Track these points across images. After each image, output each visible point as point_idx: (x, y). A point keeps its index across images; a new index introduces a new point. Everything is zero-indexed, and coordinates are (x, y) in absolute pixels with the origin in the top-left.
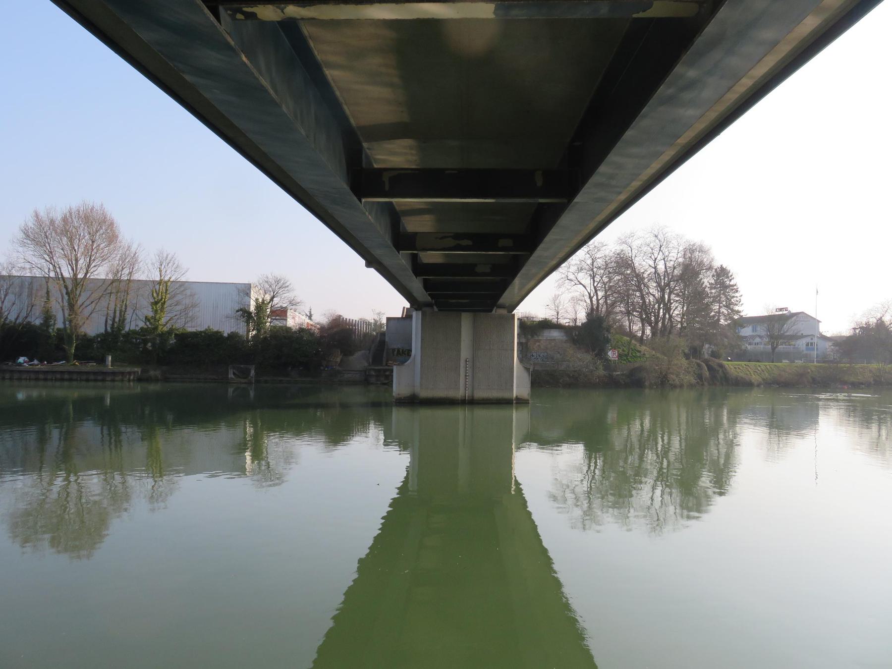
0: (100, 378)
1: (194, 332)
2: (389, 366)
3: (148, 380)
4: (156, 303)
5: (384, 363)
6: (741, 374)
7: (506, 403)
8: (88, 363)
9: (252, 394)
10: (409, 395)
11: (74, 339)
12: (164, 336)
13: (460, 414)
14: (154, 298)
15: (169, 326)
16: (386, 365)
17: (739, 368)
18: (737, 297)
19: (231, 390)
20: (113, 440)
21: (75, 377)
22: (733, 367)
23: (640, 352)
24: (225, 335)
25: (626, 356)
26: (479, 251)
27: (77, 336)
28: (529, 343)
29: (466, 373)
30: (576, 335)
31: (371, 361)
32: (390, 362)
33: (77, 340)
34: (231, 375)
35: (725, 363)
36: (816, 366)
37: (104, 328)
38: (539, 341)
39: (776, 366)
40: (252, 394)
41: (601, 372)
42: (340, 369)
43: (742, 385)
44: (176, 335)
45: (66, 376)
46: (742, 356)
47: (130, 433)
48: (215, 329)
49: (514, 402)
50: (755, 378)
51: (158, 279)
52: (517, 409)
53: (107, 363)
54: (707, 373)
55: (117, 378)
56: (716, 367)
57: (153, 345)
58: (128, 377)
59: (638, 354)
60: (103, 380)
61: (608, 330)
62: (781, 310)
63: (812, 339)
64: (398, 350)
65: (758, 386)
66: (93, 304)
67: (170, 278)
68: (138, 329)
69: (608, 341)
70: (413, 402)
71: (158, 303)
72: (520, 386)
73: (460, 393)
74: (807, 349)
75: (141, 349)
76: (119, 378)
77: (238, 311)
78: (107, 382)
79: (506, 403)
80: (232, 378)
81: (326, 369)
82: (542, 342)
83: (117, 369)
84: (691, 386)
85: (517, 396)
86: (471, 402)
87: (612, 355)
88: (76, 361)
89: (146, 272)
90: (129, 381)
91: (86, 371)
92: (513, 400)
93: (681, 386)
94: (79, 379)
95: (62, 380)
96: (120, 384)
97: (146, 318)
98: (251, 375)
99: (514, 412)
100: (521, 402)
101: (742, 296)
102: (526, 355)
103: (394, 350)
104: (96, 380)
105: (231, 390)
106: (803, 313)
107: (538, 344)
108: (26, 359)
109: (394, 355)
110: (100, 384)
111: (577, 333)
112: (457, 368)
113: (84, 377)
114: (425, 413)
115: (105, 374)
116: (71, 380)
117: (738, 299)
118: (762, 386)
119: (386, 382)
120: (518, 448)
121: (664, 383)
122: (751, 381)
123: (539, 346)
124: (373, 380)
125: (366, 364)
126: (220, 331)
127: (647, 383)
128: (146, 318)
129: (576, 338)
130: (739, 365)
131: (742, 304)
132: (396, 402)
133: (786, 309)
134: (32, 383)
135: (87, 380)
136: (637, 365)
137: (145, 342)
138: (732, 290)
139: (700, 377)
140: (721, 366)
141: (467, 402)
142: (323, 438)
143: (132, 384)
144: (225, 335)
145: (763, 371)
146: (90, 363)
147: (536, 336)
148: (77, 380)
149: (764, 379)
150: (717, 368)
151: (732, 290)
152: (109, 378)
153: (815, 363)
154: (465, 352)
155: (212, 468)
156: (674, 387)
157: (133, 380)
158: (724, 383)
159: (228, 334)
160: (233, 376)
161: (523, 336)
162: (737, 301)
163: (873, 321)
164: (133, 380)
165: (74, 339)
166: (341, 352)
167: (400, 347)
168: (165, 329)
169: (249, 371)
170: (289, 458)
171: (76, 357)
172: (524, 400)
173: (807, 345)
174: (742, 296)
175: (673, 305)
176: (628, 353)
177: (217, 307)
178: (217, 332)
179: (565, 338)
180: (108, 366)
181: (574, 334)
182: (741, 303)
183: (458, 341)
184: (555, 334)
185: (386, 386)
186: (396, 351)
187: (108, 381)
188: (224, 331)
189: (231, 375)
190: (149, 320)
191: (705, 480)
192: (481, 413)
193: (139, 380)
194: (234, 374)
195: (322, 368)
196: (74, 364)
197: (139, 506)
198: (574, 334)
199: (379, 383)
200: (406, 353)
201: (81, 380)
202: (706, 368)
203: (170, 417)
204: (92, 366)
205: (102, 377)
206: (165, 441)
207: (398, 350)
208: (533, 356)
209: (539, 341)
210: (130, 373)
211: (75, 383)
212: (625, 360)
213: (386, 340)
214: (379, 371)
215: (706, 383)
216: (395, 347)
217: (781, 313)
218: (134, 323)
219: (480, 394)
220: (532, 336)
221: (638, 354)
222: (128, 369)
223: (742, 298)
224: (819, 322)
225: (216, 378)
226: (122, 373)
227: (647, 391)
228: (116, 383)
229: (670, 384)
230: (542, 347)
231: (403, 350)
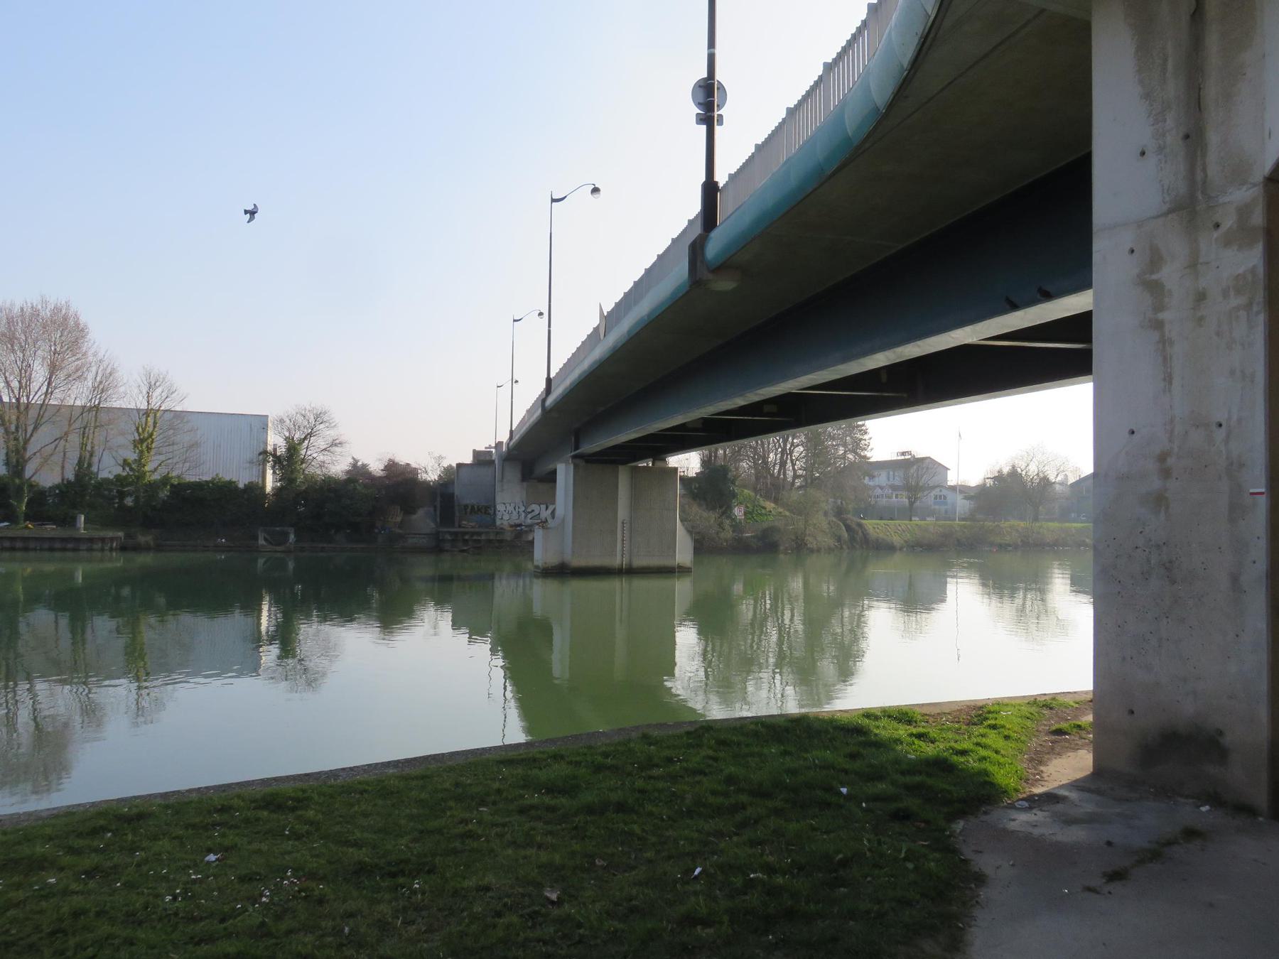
0: (70, 546)
1: (196, 482)
2: (464, 527)
3: (137, 548)
4: (142, 441)
5: (457, 524)
6: (881, 535)
8: (44, 525)
9: (291, 565)
11: (26, 492)
12: (154, 487)
13: (616, 586)
14: (139, 435)
15: (163, 471)
16: (460, 526)
17: (878, 528)
18: (865, 440)
19: (261, 562)
21: (32, 545)
22: (873, 526)
23: (765, 508)
24: (241, 486)
25: (751, 513)
26: (745, 416)
27: (31, 486)
29: (623, 537)
31: (438, 520)
32: (464, 522)
33: (29, 491)
34: (261, 542)
35: (864, 522)
36: (958, 525)
37: (32, 474)
39: (917, 525)
40: (291, 565)
41: (728, 534)
42: (400, 531)
43: (883, 548)
44: (172, 486)
46: (886, 514)
47: (102, 626)
48: (227, 479)
50: (897, 540)
51: (144, 406)
52: (678, 579)
53: (78, 525)
54: (845, 535)
55: (95, 546)
56: (854, 526)
57: (137, 500)
58: (109, 545)
59: (763, 511)
60: (75, 550)
61: (733, 482)
62: (903, 454)
63: (941, 491)
64: (473, 507)
65: (901, 549)
66: (58, 441)
67: (160, 407)
68: (111, 477)
69: (734, 495)
71: (143, 442)
72: (683, 553)
73: (617, 561)
74: (935, 504)
75: (116, 505)
76: (98, 546)
78: (81, 552)
80: (263, 545)
81: (383, 532)
84: (830, 550)
85: (678, 564)
86: (630, 572)
87: (738, 512)
88: (28, 522)
89: (129, 397)
91: (50, 536)
93: (819, 550)
94: (38, 548)
95: (13, 549)
96: (99, 554)
97: (125, 461)
98: (291, 541)
100: (682, 571)
101: (871, 438)
103: (466, 506)
104: (64, 550)
105: (261, 562)
106: (929, 458)
109: (466, 513)
110: (70, 554)
111: (697, 486)
112: (614, 532)
113: (46, 546)
114: (577, 585)
115: (78, 540)
116: (26, 549)
117: (866, 443)
118: (905, 549)
119: (465, 548)
121: (800, 547)
122: (893, 543)
124: (447, 546)
125: (433, 525)
126: (234, 480)
127: (782, 548)
128: (125, 461)
129: (696, 491)
130: (878, 524)
131: (872, 449)
133: (909, 453)
134: (47, 554)
135: (51, 549)
136: (765, 525)
137: (122, 495)
138: (860, 431)
139: (839, 539)
140: (860, 525)
141: (624, 571)
142: (976, 581)
143: (114, 554)
144: (241, 486)
145: (904, 531)
146: (47, 524)
148: (35, 550)
149: (906, 542)
150: (857, 528)
151: (860, 431)
152: (83, 547)
153: (957, 522)
154: (623, 512)
155: (222, 667)
156: (812, 551)
157: (116, 549)
158: (865, 547)
159: (245, 485)
160: (264, 543)
162: (865, 445)
163: (1006, 470)
164: (116, 549)
165: (26, 492)
166: (401, 510)
167: (475, 503)
168: (156, 477)
169: (286, 535)
170: (329, 651)
171: (28, 517)
172: (686, 568)
173: (936, 498)
174: (871, 438)
175: (797, 449)
176: (753, 510)
177: (220, 447)
178: (231, 482)
180: (79, 529)
181: (693, 487)
182: (870, 447)
185: (465, 554)
186: (470, 508)
187: (83, 550)
188: (239, 481)
189: (261, 542)
190: (129, 465)
191: (827, 667)
192: (640, 584)
193: (123, 549)
194: (266, 539)
195: (376, 531)
196: (27, 527)
197: (117, 725)
198: (693, 487)
199: (455, 549)
200: (483, 511)
201: (41, 550)
202: (844, 528)
203: (161, 601)
204: (50, 530)
205: (73, 545)
206: (150, 630)
210: (112, 539)
211: (32, 554)
212: (750, 519)
213: (456, 493)
214: (456, 534)
215: (844, 547)
216: (468, 502)
217: (903, 457)
218: (107, 468)
219: (639, 562)
221: (763, 511)
223: (871, 441)
224: (947, 469)
225: (232, 545)
226: (103, 540)
227: (782, 556)
228: (94, 554)
229: (808, 549)
231: (478, 507)
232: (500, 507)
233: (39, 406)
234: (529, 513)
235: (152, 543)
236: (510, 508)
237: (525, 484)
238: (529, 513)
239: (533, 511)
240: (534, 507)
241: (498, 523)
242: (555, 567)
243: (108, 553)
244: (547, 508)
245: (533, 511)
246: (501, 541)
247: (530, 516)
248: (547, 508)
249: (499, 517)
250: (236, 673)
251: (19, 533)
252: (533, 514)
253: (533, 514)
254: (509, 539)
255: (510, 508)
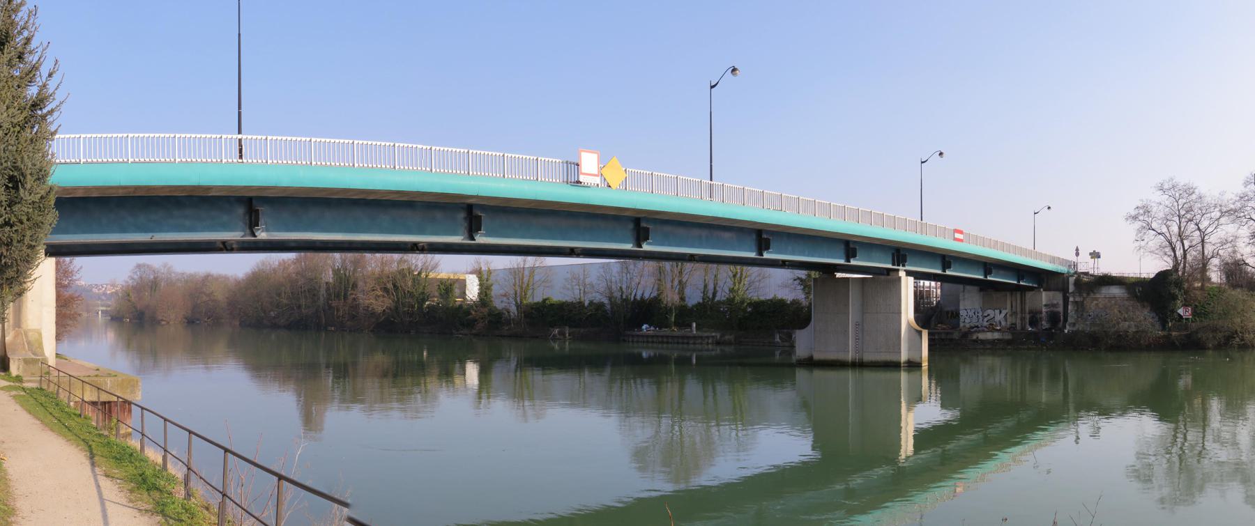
0: (686, 341)
7: (894, 366)
10: (806, 357)
13: (850, 375)
20: (624, 391)
28: (1085, 302)
30: (1139, 291)
38: (1096, 299)
45: (665, 340)
49: (902, 365)
55: (697, 342)
57: (1068, 332)
70: (810, 363)
73: (850, 356)
77: (795, 280)
79: (894, 366)
80: (778, 342)
82: (1100, 300)
83: (700, 334)
86: (859, 365)
90: (708, 344)
92: (900, 363)
99: (850, 374)
102: (1082, 315)
103: (948, 312)
107: (1095, 302)
108: (647, 326)
111: (1141, 289)
112: (846, 332)
113: (676, 340)
120: (909, 409)
123: (1097, 304)
129: (1139, 294)
132: (900, 367)
147: (1092, 294)
152: (691, 342)
160: (778, 340)
161: (1077, 294)
171: (676, 324)
172: (915, 363)
179: (1126, 295)
181: (1137, 290)
183: (847, 305)
184: (1116, 291)
189: (778, 339)
192: (869, 375)
193: (718, 343)
194: (780, 338)
196: (673, 330)
198: (1137, 290)
207: (952, 313)
208: (1090, 316)
209: (1096, 299)
219: (868, 357)
220: (1088, 294)
222: (706, 334)
228: (697, 346)
230: (1101, 306)
232: (962, 313)
233: (947, 285)
234: (986, 317)
235: (733, 340)
236: (971, 314)
237: (982, 293)
238: (986, 317)
239: (989, 315)
240: (989, 311)
241: (962, 325)
242: (805, 359)
243: (631, 344)
244: (1000, 312)
245: (989, 315)
246: (951, 340)
247: (986, 319)
248: (1000, 312)
249: (962, 320)
250: (729, 421)
251: (662, 334)
252: (988, 318)
253: (988, 318)
254: (957, 338)
255: (971, 314)
